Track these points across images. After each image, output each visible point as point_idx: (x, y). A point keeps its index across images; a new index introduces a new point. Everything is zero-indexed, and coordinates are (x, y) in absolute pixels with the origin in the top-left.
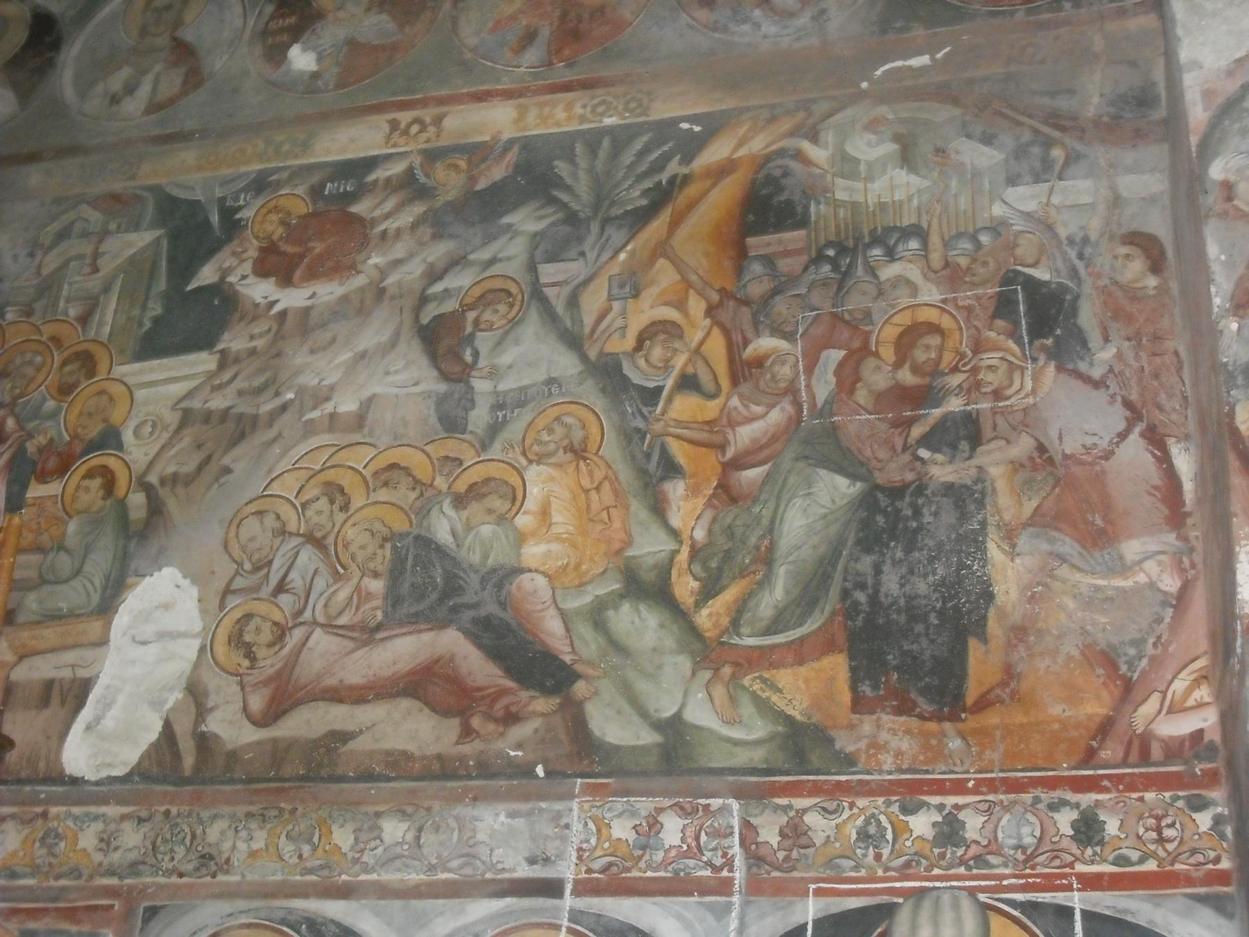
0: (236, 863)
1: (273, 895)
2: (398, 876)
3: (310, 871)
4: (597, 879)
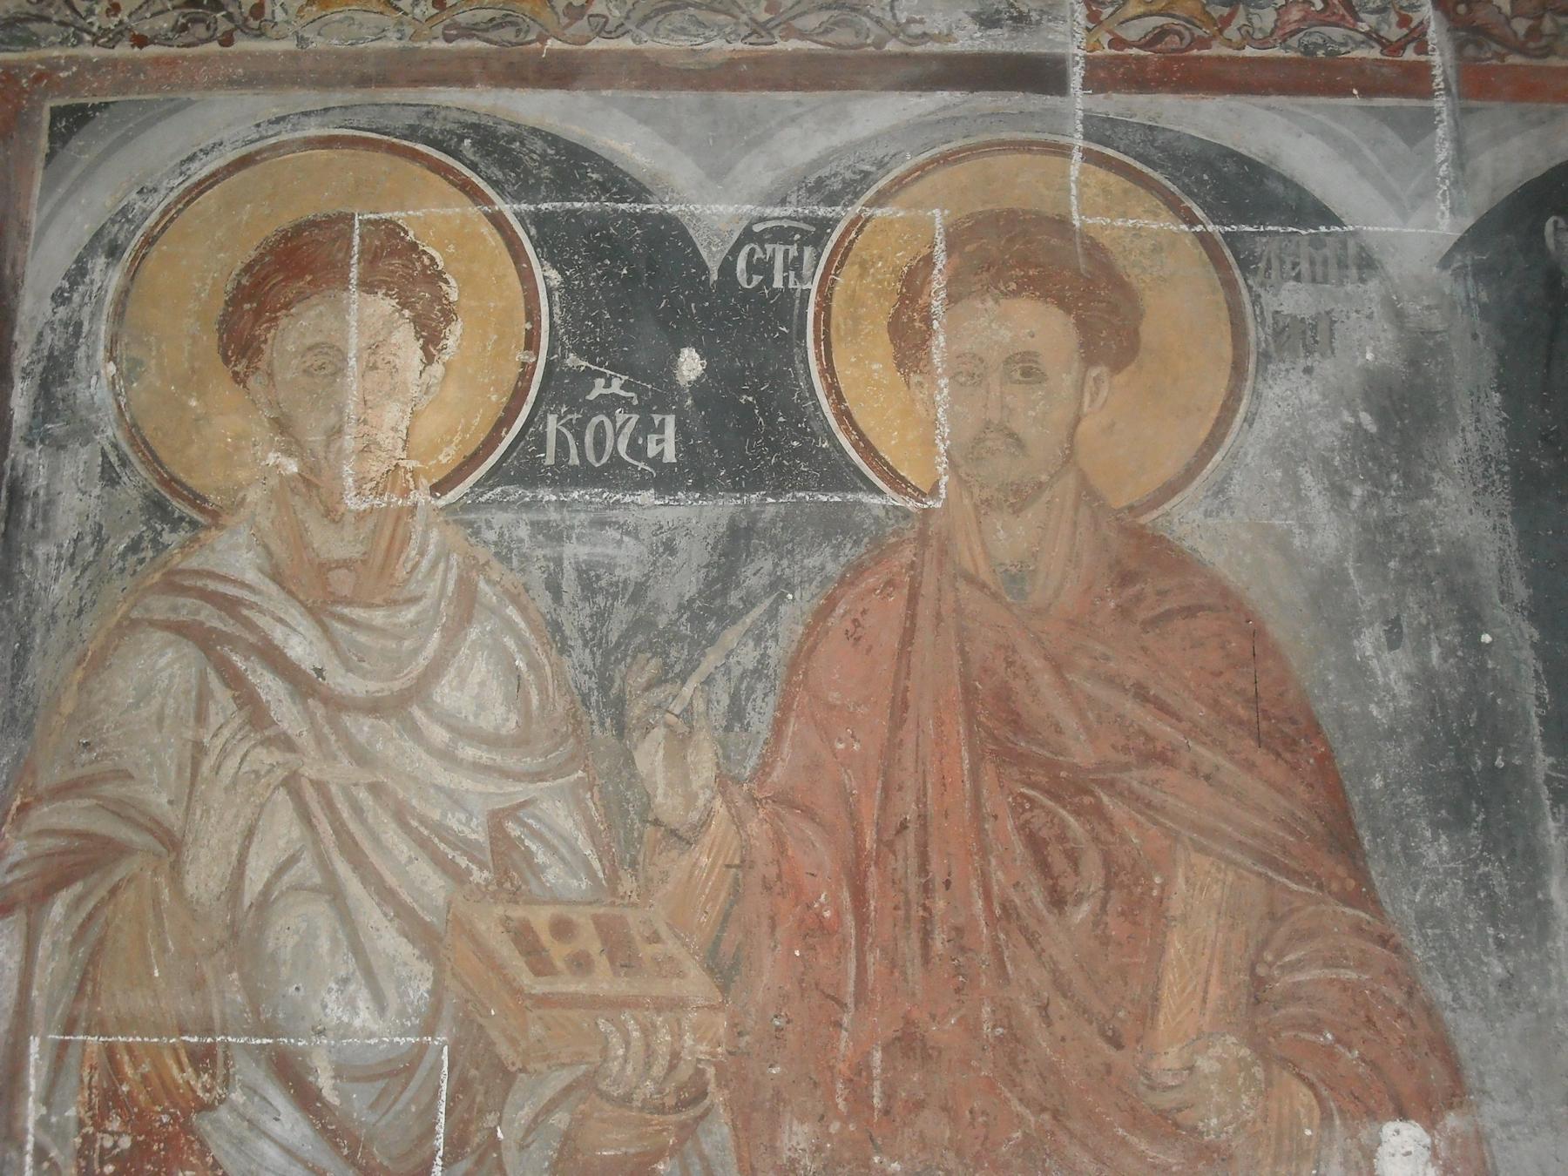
0: (280, 16)
1: (384, 81)
2: (683, 43)
3: (469, 31)
4: (1138, 59)
